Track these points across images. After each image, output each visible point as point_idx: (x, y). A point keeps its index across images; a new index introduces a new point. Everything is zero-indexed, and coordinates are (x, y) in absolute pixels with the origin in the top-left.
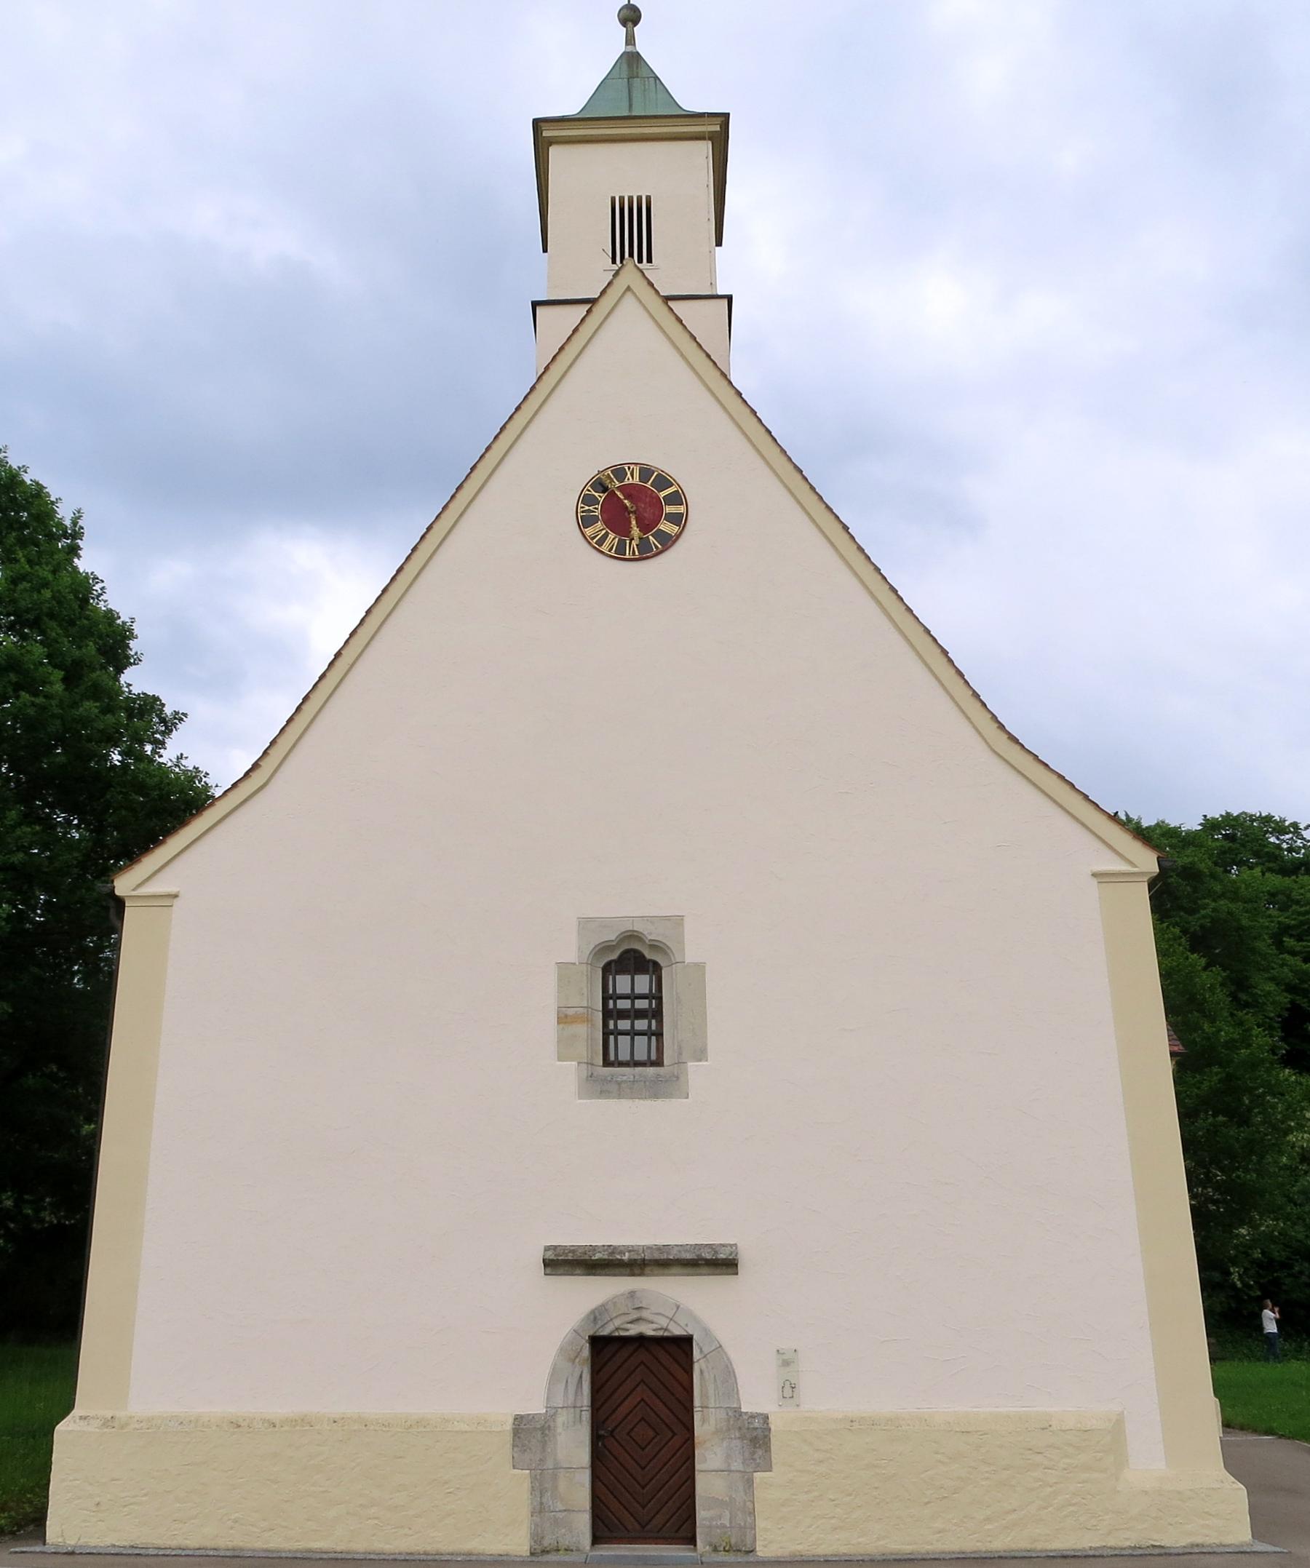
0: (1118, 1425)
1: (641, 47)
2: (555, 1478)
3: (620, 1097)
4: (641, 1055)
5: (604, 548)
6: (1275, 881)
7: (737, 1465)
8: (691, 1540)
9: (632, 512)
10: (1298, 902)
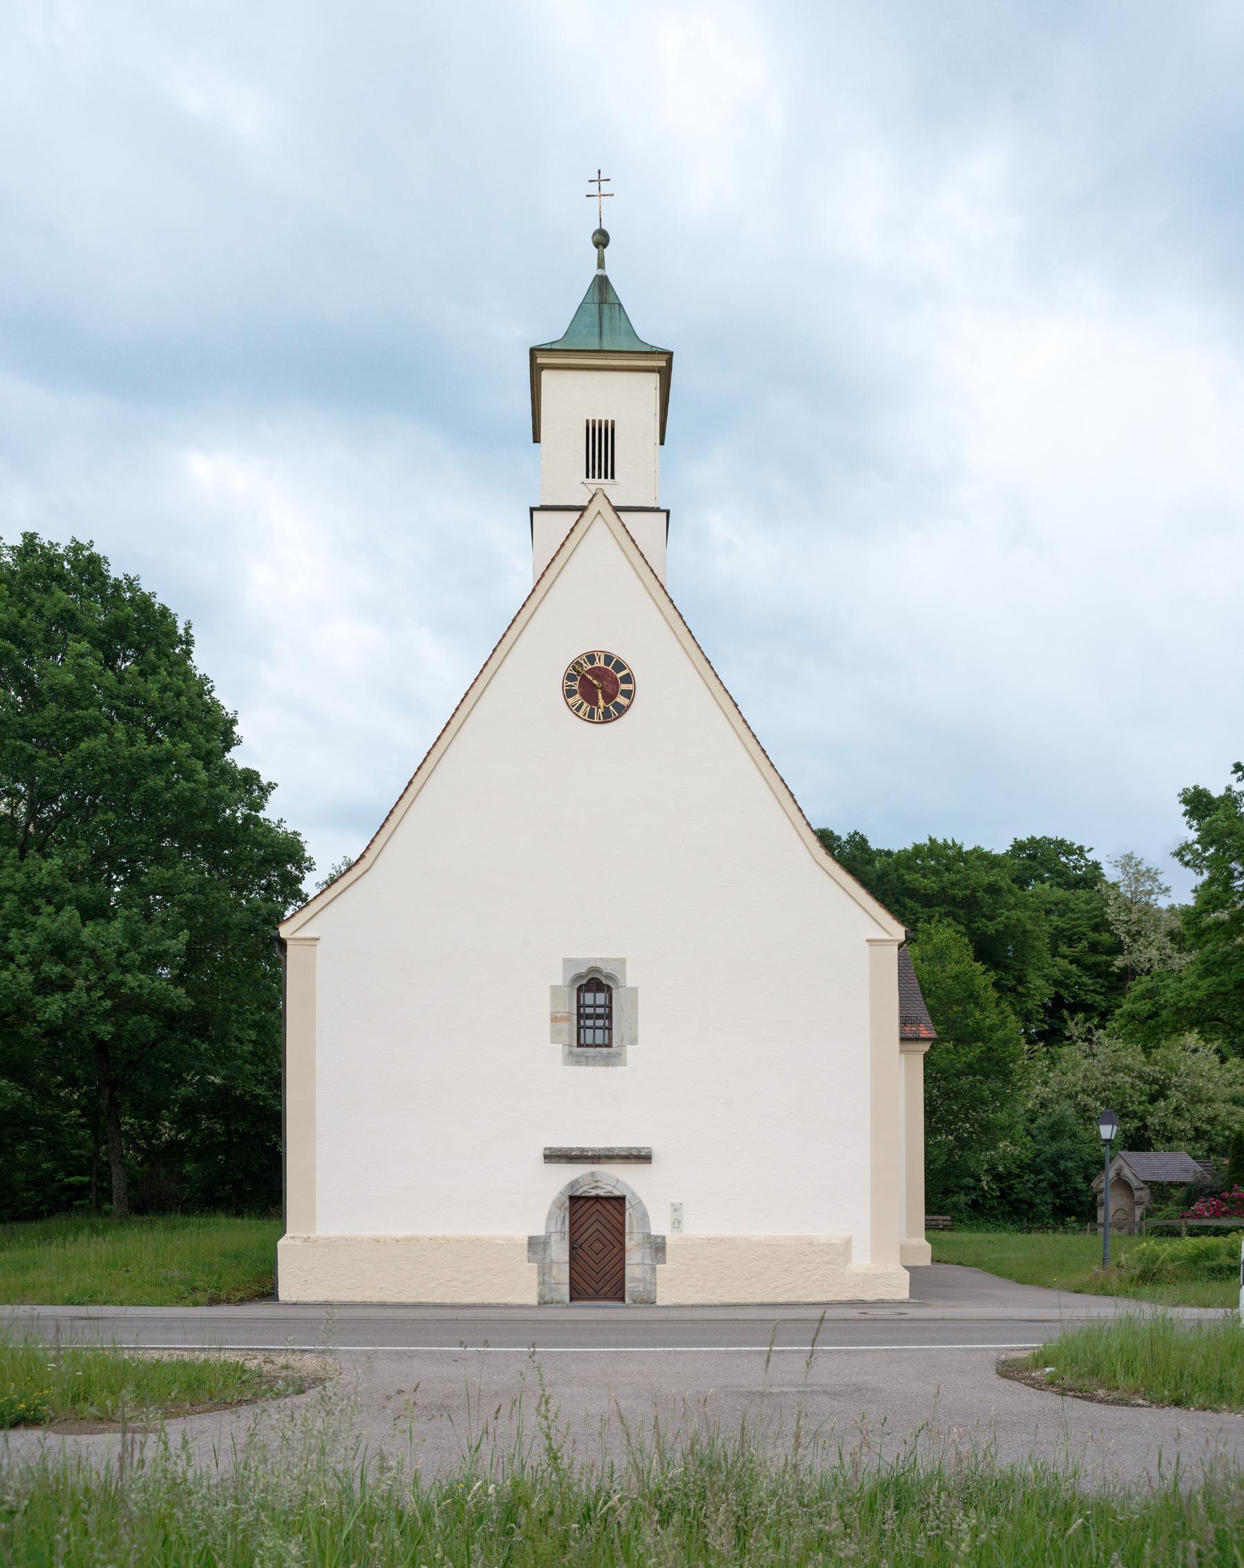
0: (848, 1243)
1: (609, 272)
2: (550, 1268)
3: (587, 1065)
4: (599, 1041)
5: (581, 714)
6: (1060, 893)
7: (648, 1261)
8: (623, 1299)
9: (599, 687)
10: (1072, 911)
